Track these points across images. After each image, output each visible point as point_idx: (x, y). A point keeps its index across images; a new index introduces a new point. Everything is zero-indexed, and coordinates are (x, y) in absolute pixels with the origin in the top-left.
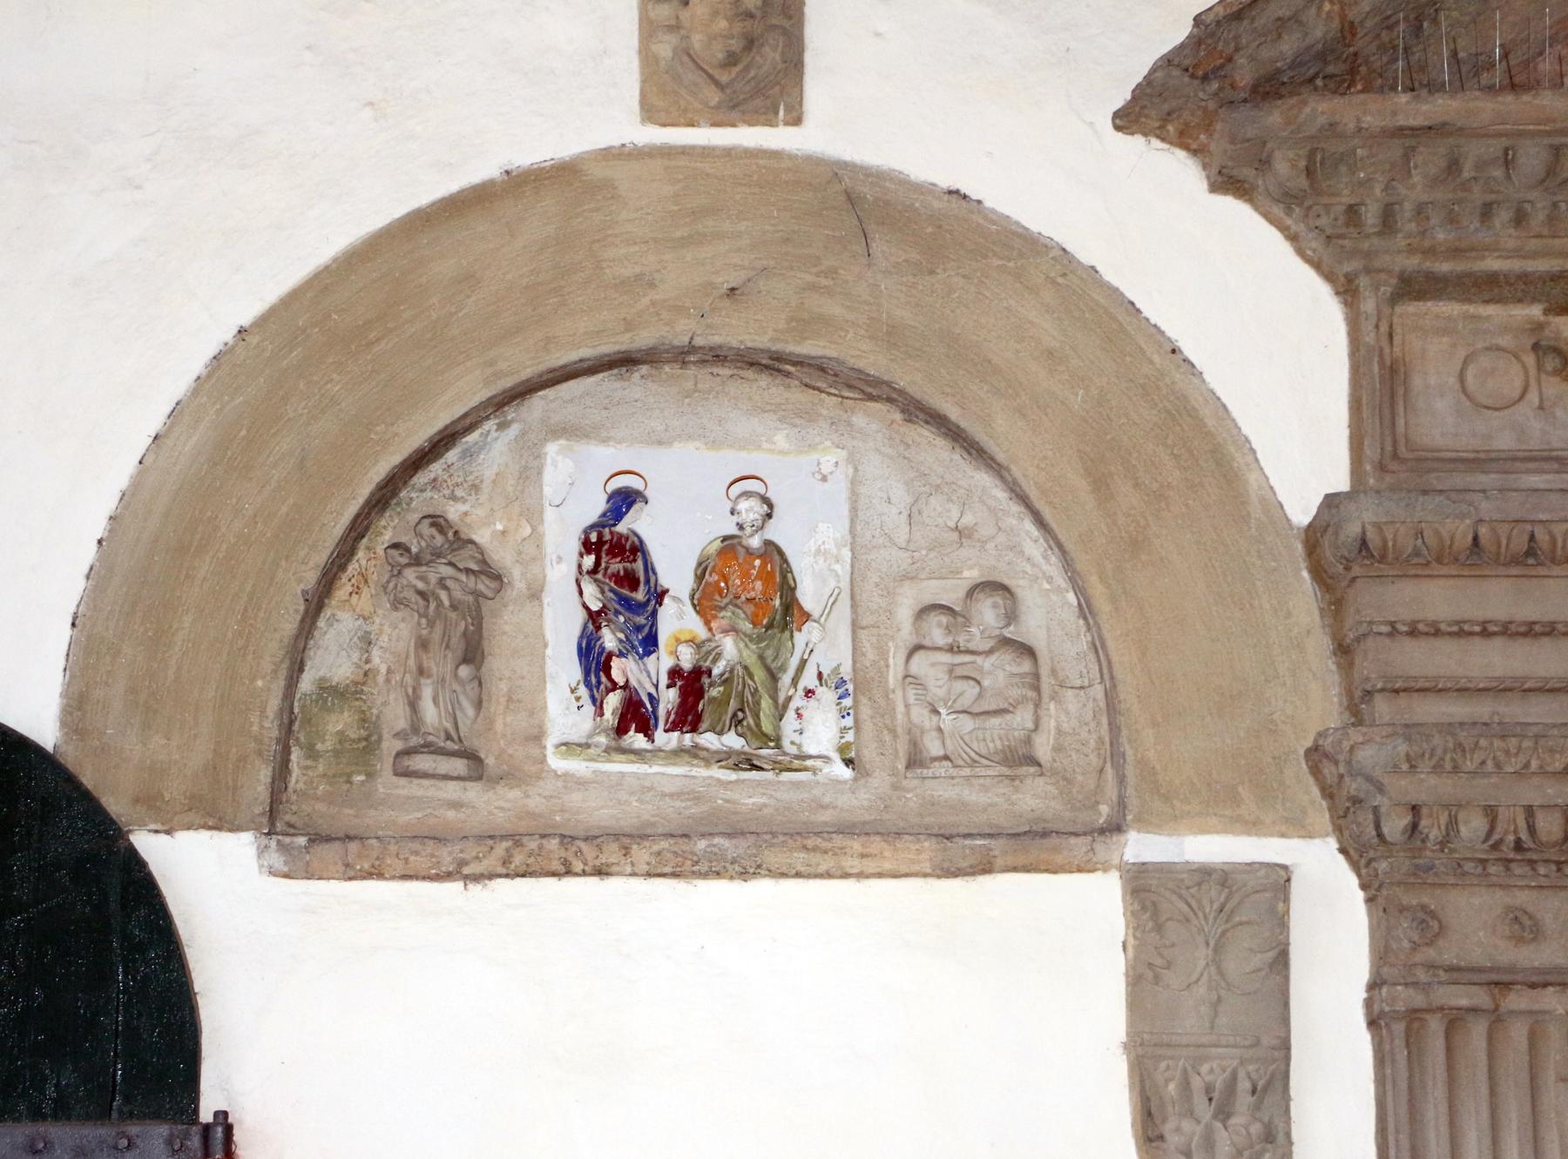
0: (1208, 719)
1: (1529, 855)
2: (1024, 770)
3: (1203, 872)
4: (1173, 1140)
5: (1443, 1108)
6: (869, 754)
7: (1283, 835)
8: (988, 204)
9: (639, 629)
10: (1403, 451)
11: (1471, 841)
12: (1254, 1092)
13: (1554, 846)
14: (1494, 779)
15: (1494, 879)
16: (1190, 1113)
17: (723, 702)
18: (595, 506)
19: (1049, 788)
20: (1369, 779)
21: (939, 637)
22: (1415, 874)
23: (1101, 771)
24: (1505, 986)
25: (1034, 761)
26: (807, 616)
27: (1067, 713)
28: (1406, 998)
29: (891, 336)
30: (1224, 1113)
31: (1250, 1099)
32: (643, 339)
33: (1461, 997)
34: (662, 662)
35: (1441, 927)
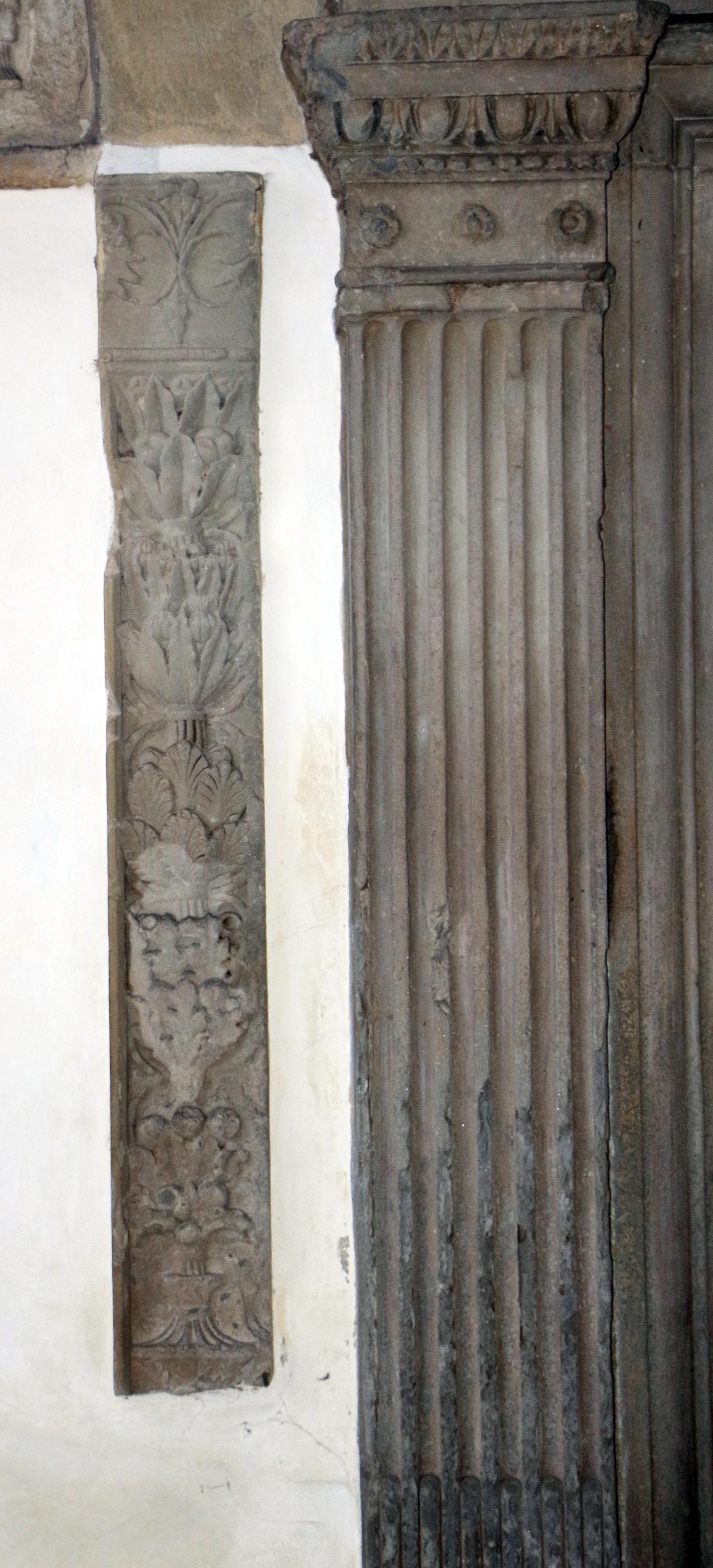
0: (184, 21)
1: (494, 150)
3: (175, 183)
4: (143, 455)
5: (396, 411)
7: (258, 144)
11: (431, 135)
12: (222, 404)
13: (514, 138)
14: (457, 69)
15: (455, 176)
16: (161, 430)
19: (30, 102)
20: (330, 73)
22: (376, 175)
23: (82, 83)
24: (460, 285)
27: (48, 22)
30: (192, 427)
31: (219, 412)
33: (416, 298)
35: (400, 228)
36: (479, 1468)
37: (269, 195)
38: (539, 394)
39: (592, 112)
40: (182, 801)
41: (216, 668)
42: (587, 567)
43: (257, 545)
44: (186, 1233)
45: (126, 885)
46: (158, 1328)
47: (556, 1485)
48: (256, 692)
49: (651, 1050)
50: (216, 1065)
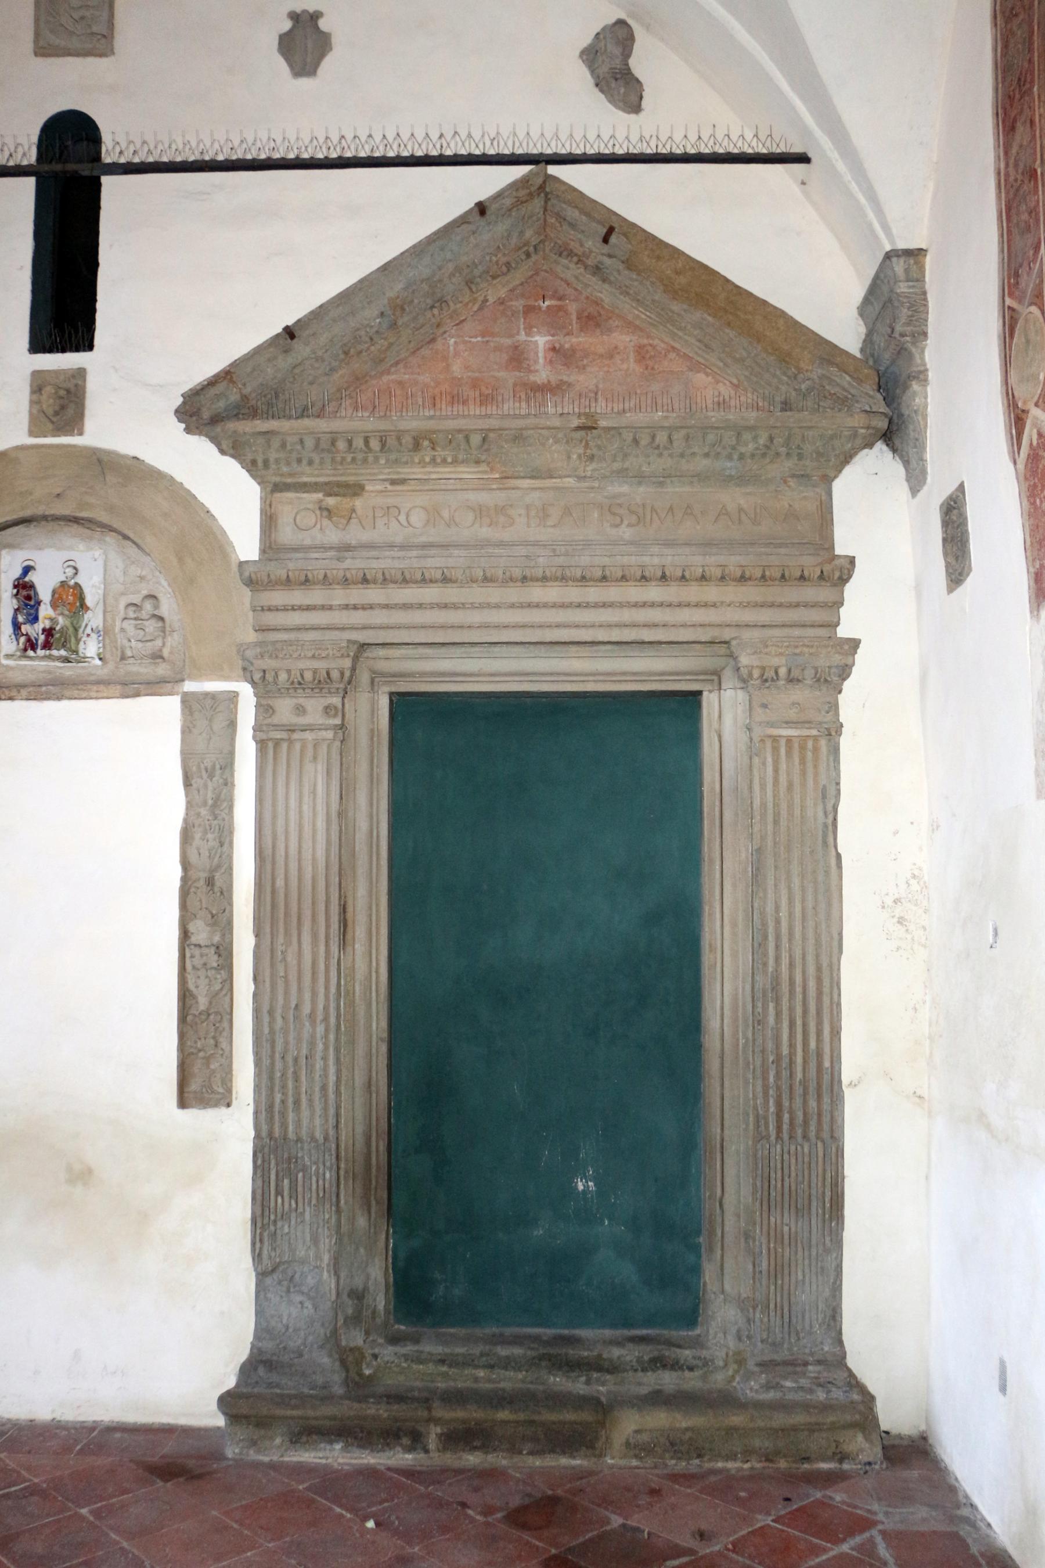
2: (158, 661)
4: (195, 786)
6: (108, 656)
8: (147, 461)
9: (30, 615)
10: (273, 546)
17: (59, 639)
18: (17, 572)
21: (132, 615)
24: (293, 731)
25: (162, 657)
26: (88, 608)
28: (262, 736)
29: (111, 509)
30: (211, 776)
32: (27, 513)
33: (278, 735)
34: (40, 626)
36: (291, 1135)
37: (240, 698)
38: (319, 767)
39: (335, 675)
40: (204, 906)
41: (216, 860)
42: (335, 827)
43: (232, 817)
44: (201, 1054)
45: (185, 935)
46: (194, 1086)
47: (316, 1141)
48: (231, 868)
49: (357, 994)
50: (214, 996)
